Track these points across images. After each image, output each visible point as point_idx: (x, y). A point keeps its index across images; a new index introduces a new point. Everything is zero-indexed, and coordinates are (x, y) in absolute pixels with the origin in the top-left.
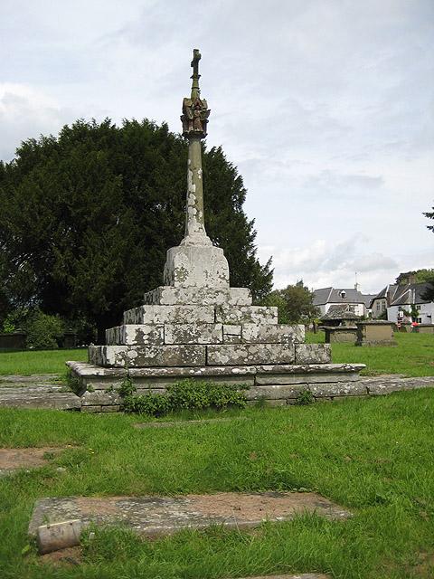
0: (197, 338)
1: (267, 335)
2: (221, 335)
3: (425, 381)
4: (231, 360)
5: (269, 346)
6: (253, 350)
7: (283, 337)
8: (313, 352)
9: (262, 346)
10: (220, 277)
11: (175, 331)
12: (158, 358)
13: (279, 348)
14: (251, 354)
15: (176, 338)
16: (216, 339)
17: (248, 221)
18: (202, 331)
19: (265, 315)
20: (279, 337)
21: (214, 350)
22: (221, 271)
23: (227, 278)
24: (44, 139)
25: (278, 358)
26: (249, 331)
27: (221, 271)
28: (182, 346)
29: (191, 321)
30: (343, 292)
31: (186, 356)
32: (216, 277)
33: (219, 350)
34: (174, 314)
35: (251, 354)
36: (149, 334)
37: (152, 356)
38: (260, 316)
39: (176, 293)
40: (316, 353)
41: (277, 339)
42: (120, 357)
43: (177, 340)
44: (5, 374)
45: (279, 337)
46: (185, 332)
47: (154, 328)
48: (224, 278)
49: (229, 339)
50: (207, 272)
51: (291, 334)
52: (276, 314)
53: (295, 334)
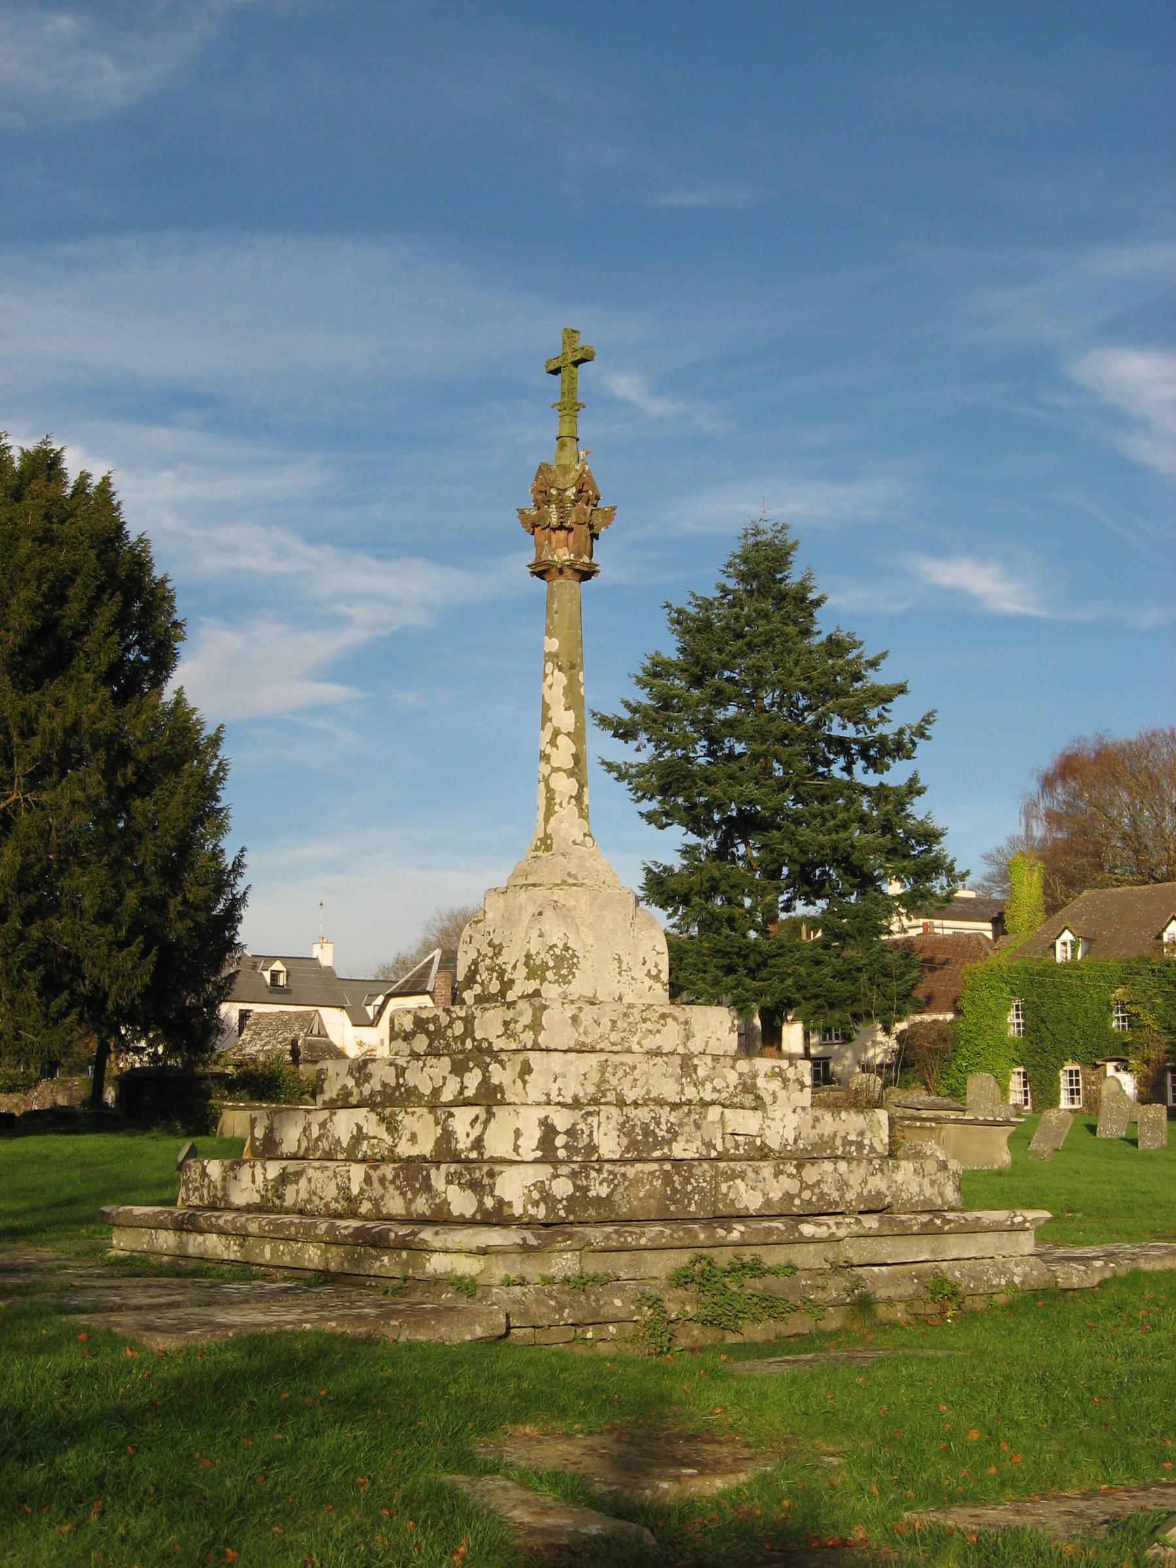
0: (669, 1142)
1: (813, 1135)
2: (719, 1135)
3: (1170, 1263)
4: (768, 1202)
5: (842, 1166)
6: (811, 1174)
7: (846, 1143)
8: (926, 1181)
9: (828, 1166)
10: (648, 974)
11: (623, 1125)
12: (617, 1197)
13: (861, 1171)
14: (808, 1187)
15: (625, 1141)
16: (710, 1145)
17: (208, 731)
18: (681, 1125)
19: (785, 1081)
20: (838, 1142)
21: (732, 1176)
22: (652, 958)
23: (665, 977)
24: (163, 582)
25: (860, 1195)
26: (777, 1126)
27: (652, 958)
28: (667, 1167)
29: (630, 1096)
30: (278, 966)
31: (675, 1190)
32: (640, 973)
33: (742, 1175)
34: (595, 1077)
35: (808, 1187)
36: (567, 1133)
37: (604, 1191)
38: (775, 1085)
39: (575, 1019)
40: (933, 1183)
41: (833, 1148)
42: (536, 1195)
43: (628, 1149)
44: (14, 1233)
45: (838, 1142)
46: (646, 1126)
47: (578, 1114)
48: (657, 978)
49: (737, 1147)
50: (620, 961)
51: (861, 1134)
52: (808, 1080)
53: (868, 1134)
